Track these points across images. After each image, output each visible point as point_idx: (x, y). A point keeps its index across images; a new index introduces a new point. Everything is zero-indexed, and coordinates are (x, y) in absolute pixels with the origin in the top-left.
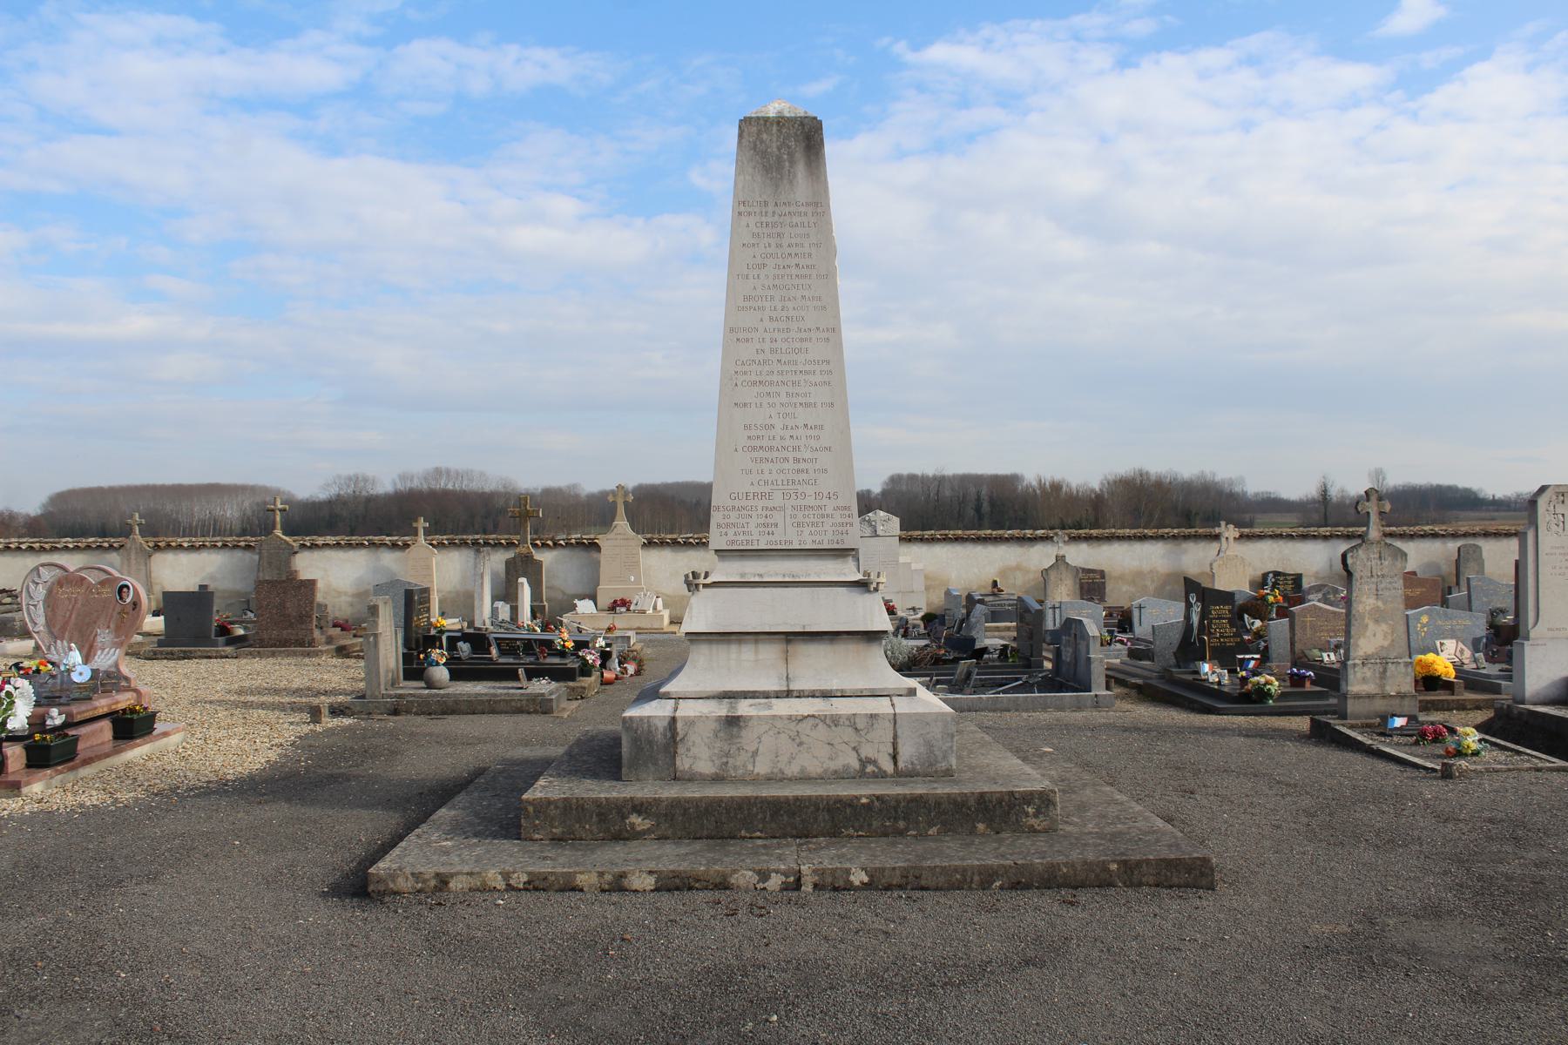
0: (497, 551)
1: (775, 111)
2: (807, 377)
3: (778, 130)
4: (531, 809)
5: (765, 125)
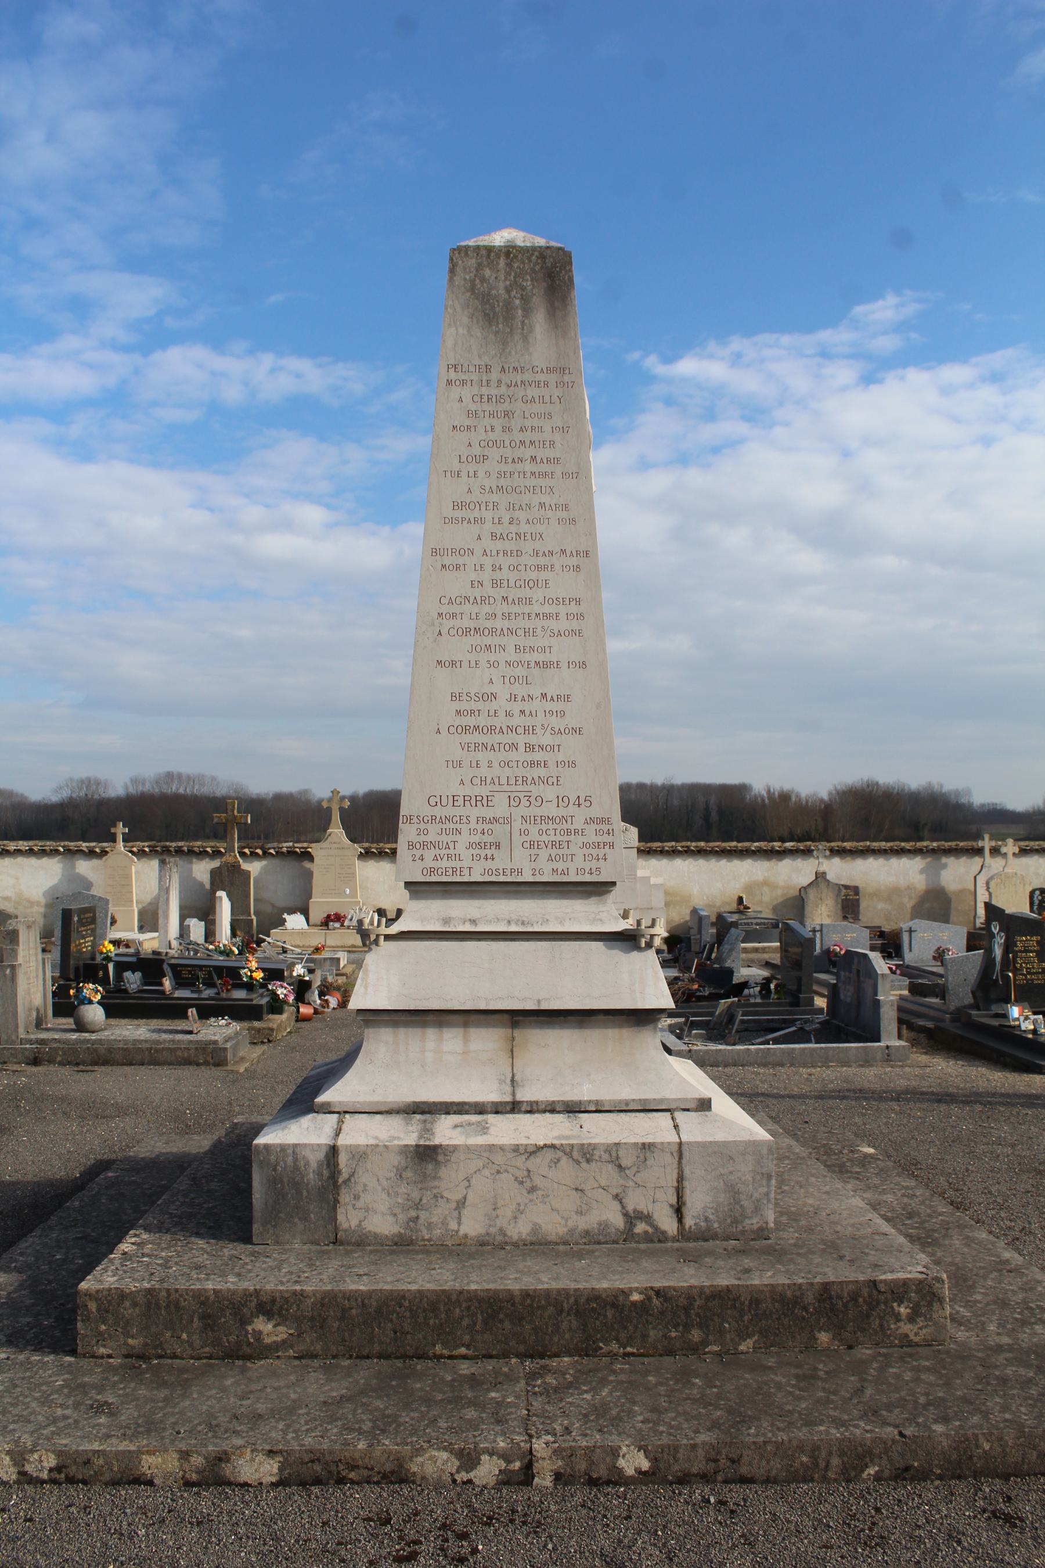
0: (202, 860)
1: (504, 240)
2: (546, 623)
3: (507, 264)
4: (93, 1306)
5: (488, 256)
